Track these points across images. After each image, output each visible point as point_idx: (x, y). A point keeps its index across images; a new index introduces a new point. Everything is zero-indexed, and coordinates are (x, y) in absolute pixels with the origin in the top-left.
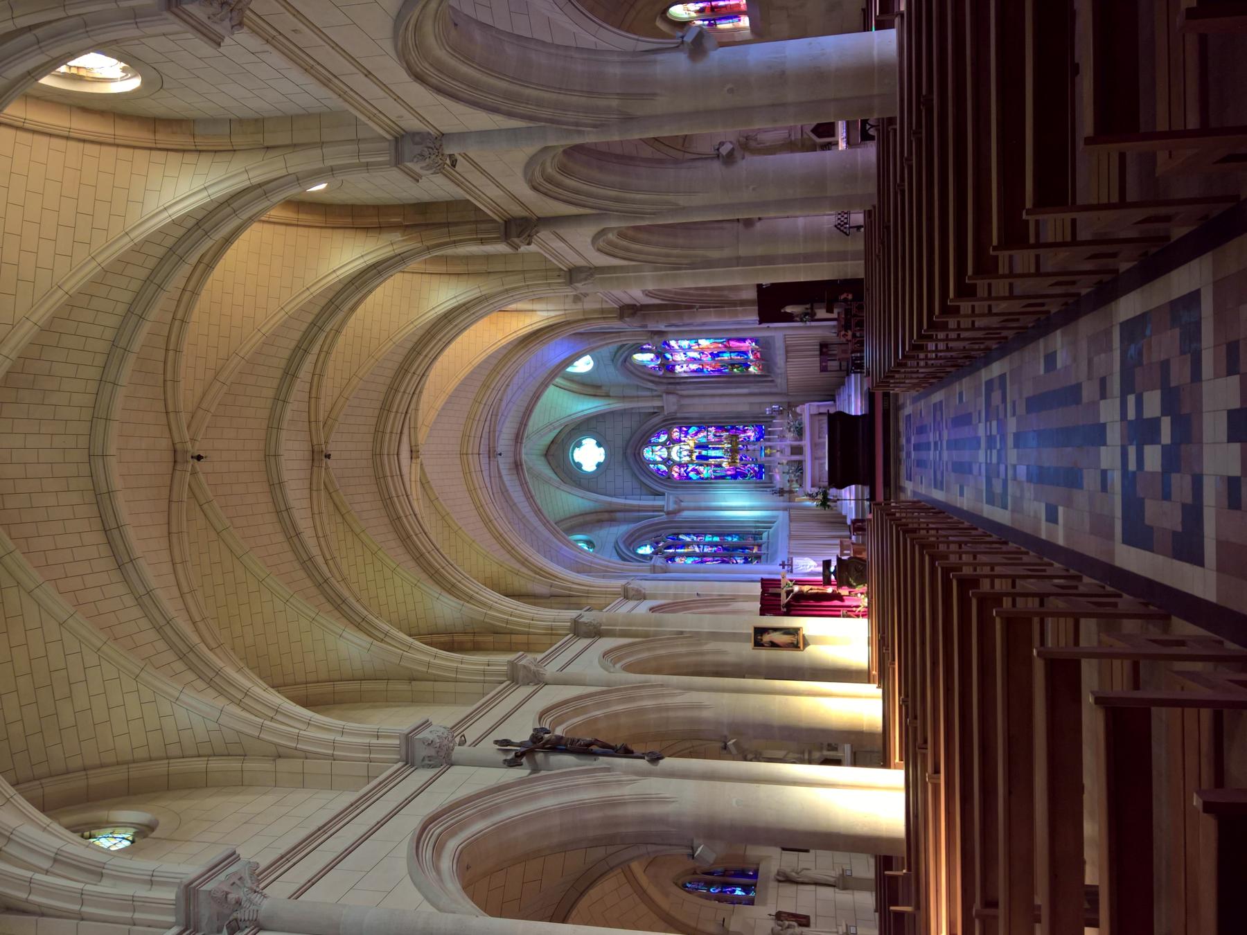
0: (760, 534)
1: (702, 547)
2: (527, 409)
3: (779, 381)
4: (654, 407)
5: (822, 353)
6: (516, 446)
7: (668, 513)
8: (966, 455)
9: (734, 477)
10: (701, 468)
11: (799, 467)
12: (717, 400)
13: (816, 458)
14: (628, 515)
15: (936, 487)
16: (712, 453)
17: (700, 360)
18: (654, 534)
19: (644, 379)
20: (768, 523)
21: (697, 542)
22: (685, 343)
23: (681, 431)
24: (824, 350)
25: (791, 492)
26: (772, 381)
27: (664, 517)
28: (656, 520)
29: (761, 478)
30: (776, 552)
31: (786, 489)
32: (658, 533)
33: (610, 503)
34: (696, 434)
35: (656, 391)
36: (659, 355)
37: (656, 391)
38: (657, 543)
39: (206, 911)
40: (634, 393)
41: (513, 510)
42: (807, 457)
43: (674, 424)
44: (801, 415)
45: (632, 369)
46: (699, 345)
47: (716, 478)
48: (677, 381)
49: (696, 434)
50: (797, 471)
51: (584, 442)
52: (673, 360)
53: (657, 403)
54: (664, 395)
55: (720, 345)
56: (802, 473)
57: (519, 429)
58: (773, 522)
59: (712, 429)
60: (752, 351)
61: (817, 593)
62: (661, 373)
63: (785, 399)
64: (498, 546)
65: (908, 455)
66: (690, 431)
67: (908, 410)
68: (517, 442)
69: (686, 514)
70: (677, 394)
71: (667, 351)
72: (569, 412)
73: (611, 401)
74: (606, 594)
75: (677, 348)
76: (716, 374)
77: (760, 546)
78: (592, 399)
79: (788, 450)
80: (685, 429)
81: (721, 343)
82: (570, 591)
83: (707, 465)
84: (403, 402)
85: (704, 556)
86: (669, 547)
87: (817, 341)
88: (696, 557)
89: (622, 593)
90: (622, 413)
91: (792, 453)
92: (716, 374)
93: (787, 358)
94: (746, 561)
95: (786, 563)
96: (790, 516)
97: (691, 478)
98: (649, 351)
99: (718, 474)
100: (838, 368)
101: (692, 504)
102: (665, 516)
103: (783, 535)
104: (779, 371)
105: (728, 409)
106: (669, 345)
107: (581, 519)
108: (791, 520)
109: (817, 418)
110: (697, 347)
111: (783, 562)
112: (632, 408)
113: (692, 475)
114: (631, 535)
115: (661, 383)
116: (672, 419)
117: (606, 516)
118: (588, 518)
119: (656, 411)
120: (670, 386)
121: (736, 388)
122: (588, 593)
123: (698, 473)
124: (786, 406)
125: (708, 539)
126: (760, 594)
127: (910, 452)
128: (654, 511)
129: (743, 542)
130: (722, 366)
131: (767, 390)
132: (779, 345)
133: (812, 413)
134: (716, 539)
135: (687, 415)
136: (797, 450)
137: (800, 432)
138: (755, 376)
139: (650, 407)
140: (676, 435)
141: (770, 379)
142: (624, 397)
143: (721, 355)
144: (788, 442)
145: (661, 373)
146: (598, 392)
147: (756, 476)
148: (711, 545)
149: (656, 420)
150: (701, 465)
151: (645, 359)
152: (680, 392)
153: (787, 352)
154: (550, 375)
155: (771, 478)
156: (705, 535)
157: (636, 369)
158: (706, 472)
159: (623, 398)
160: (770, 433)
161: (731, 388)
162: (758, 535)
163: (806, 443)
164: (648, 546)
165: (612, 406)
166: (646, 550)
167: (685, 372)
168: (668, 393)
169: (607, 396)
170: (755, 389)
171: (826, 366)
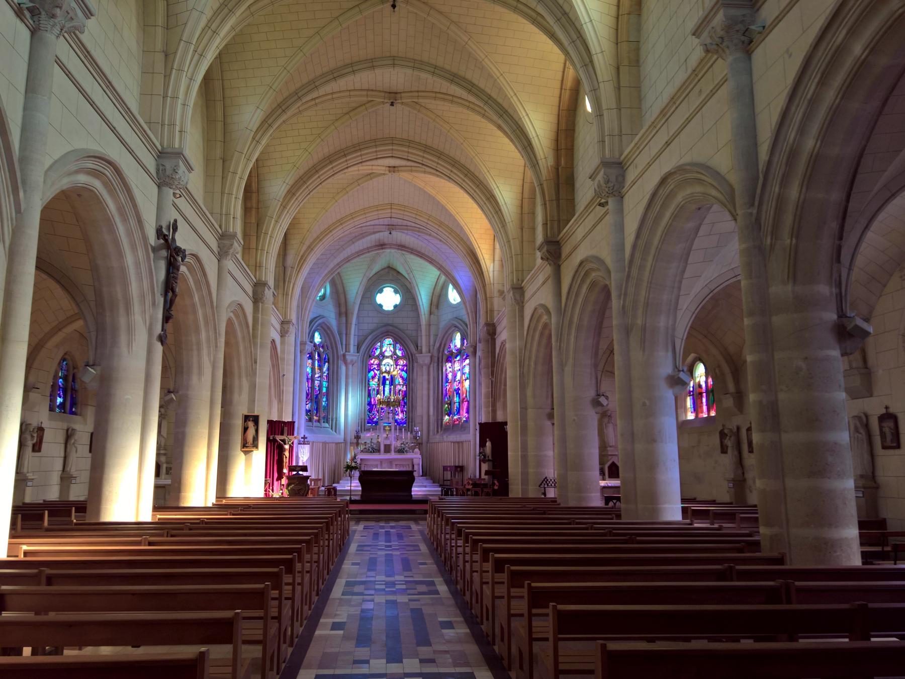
1: (319, 379)
4: (421, 347)
5: (456, 467)
7: (344, 355)
8: (381, 567)
9: (370, 404)
10: (376, 380)
12: (425, 392)
13: (381, 462)
15: (359, 546)
16: (387, 388)
18: (329, 345)
19: (442, 339)
20: (335, 427)
22: (467, 370)
23: (403, 366)
25: (358, 444)
26: (438, 432)
27: (341, 352)
28: (339, 346)
29: (368, 423)
31: (360, 441)
34: (401, 377)
35: (434, 348)
36: (459, 352)
37: (434, 348)
40: (432, 333)
43: (409, 361)
44: (413, 452)
45: (450, 331)
46: (465, 380)
47: (369, 391)
48: (440, 364)
49: (401, 377)
50: (373, 448)
52: (455, 361)
53: (424, 350)
54: (430, 354)
55: (464, 395)
56: (371, 452)
59: (404, 389)
62: (446, 352)
65: (382, 527)
67: (414, 527)
69: (343, 368)
70: (431, 364)
71: (462, 357)
72: (420, 285)
73: (427, 316)
75: (464, 364)
77: (319, 421)
79: (388, 442)
80: (405, 369)
81: (466, 396)
83: (379, 384)
86: (319, 355)
88: (312, 376)
89: (285, 320)
91: (385, 445)
92: (444, 392)
94: (308, 411)
97: (369, 372)
98: (462, 344)
101: (350, 373)
102: (342, 353)
104: (445, 437)
105: (419, 400)
106: (466, 359)
107: (340, 290)
108: (337, 444)
109: (410, 463)
110: (464, 378)
111: (306, 438)
112: (421, 331)
113: (372, 373)
114: (329, 328)
115: (439, 353)
116: (413, 360)
117: (343, 310)
118: (342, 297)
120: (436, 359)
122: (286, 295)
123: (373, 378)
124: (420, 441)
125: (325, 384)
127: (384, 529)
128: (346, 345)
129: (322, 409)
130: (449, 396)
131: (431, 428)
134: (324, 390)
136: (388, 449)
137: (400, 451)
138: (442, 420)
139: (421, 343)
141: (439, 430)
142: (430, 325)
143: (458, 395)
147: (370, 419)
148: (320, 386)
150: (379, 380)
152: (432, 365)
153: (458, 443)
155: (368, 430)
156: (328, 382)
158: (373, 383)
159: (429, 325)
160: (400, 430)
164: (320, 340)
165: (423, 316)
166: (317, 339)
167: (446, 369)
168: (431, 357)
169: (431, 313)
170: (432, 419)
171: (447, 470)
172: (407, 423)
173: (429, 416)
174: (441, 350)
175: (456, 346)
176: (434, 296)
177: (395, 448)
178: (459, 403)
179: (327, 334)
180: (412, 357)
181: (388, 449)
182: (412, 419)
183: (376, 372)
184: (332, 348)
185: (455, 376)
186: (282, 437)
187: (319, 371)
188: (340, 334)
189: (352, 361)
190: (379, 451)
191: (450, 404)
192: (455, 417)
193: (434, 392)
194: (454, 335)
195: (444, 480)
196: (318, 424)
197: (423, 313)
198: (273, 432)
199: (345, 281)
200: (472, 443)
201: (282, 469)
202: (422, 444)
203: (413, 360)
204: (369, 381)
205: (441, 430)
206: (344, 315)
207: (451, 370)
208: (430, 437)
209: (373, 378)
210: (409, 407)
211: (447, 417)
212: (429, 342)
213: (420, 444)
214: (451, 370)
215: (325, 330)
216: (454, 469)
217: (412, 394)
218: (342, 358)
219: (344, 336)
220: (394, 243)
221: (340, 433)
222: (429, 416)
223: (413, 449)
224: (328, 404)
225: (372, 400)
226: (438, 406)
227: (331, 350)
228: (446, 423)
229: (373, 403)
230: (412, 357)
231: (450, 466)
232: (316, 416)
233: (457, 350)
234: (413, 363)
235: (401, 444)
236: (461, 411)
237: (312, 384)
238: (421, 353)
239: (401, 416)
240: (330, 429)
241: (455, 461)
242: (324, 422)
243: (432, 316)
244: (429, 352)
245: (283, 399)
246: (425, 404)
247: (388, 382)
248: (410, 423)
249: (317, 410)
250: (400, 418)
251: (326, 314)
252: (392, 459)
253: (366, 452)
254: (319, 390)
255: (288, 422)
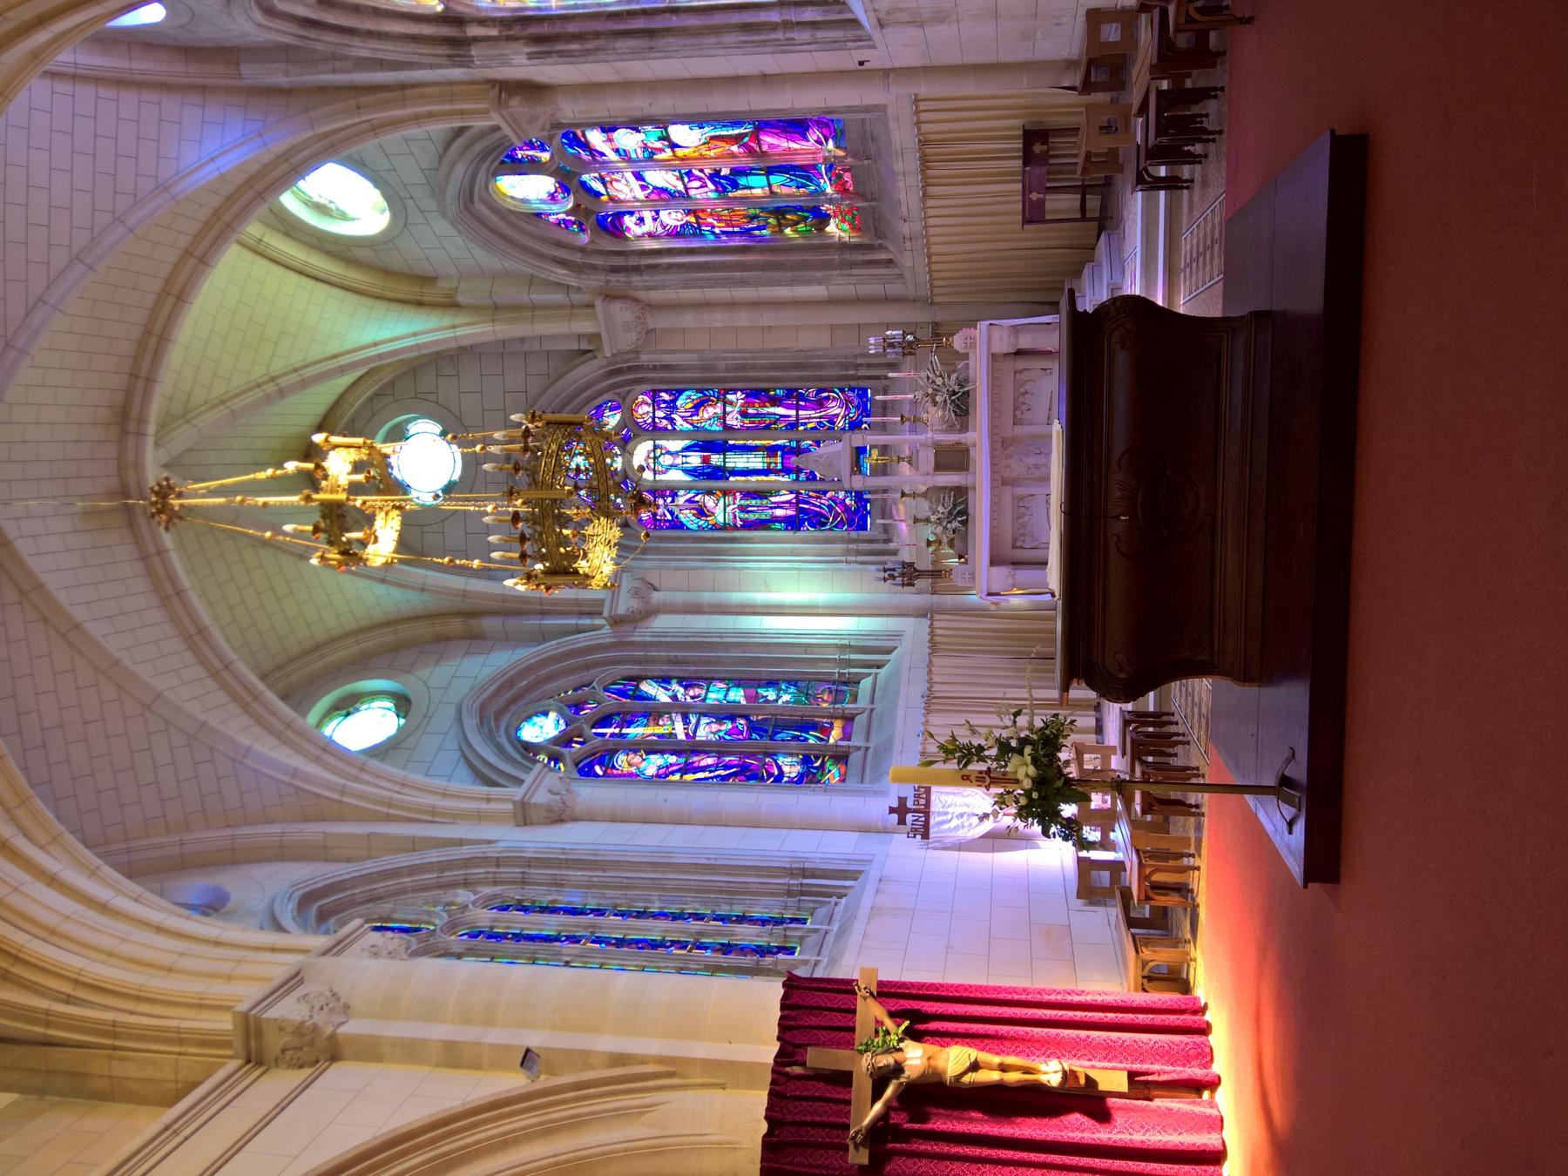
0: (854, 682)
1: (693, 719)
2: (147, 331)
3: (907, 261)
4: (579, 337)
5: (1028, 158)
6: (121, 442)
7: (616, 621)
9: (792, 524)
10: (709, 502)
11: (958, 506)
12: (742, 319)
13: (1004, 483)
14: (513, 624)
16: (737, 461)
17: (685, 195)
18: (575, 679)
19: (541, 256)
20: (875, 652)
21: (685, 705)
22: (628, 140)
23: (656, 403)
24: (1038, 148)
25: (936, 574)
26: (890, 262)
27: (606, 634)
28: (582, 640)
29: (863, 527)
30: (888, 746)
31: (924, 564)
32: (586, 676)
33: (465, 594)
34: (697, 407)
35: (579, 290)
36: (567, 182)
37: (579, 290)
38: (578, 707)
39: (251, 1020)
40: (521, 295)
41: (71, 645)
42: (980, 478)
43: (638, 381)
44: (966, 356)
45: (494, 220)
46: (674, 146)
47: (748, 525)
48: (633, 261)
49: (697, 407)
50: (951, 516)
51: (413, 428)
52: (612, 199)
53: (584, 326)
54: (598, 303)
55: (735, 148)
56: (964, 523)
57: (129, 393)
58: (889, 651)
59: (737, 398)
60: (830, 168)
61: (999, 1087)
62: (584, 238)
63: (922, 316)
64: (222, 697)
66: (679, 403)
68: (124, 432)
69: (662, 623)
70: (636, 300)
71: (587, 167)
72: (334, 347)
73: (460, 319)
74: (182, 1042)
75: (612, 156)
76: (737, 242)
77: (849, 719)
78: (409, 311)
79: (927, 458)
80: (666, 397)
81: (737, 139)
82: (47, 1024)
83: (725, 493)
84: (311, 368)
85: (695, 752)
86: (605, 721)
87: (1016, 124)
88: (673, 753)
89: (238, 1043)
90: (501, 350)
91: (939, 467)
92: (737, 242)
93: (926, 185)
94: (809, 776)
95: (910, 804)
96: (932, 634)
97: (681, 526)
98: (533, 167)
99: (751, 517)
100: (1079, 216)
101: (680, 597)
102: (607, 630)
103: (912, 692)
104: (905, 229)
105: (774, 342)
106: (586, 146)
107: (387, 637)
108: (934, 647)
109: (1011, 365)
110: (668, 154)
111: (902, 801)
112: (522, 340)
113: (687, 517)
114: (511, 683)
115: (593, 267)
116: (631, 369)
117: (455, 626)
118: (408, 632)
119: (584, 346)
120: (613, 278)
121: (793, 282)
122: (116, 1036)
123: (701, 512)
124: (925, 334)
125: (715, 695)
126: (770, 1060)
128: (582, 614)
129: (806, 708)
130: (752, 218)
131: (875, 289)
132: (902, 136)
133: (996, 350)
134: (737, 695)
135: (668, 359)
136: (952, 458)
137: (961, 406)
138: (843, 246)
139: (566, 337)
140: (644, 411)
141: (883, 256)
142: (496, 307)
143: (742, 181)
144: (930, 436)
145: (584, 238)
146: (429, 294)
147: (850, 523)
148: (722, 714)
149: (588, 370)
150: (710, 493)
151: (532, 196)
152: (641, 295)
153: (925, 162)
154: (207, 226)
155: (888, 533)
156: (710, 680)
157: (512, 225)
158: (721, 510)
159: (495, 310)
160: (885, 408)
161: (779, 283)
162: (844, 686)
163: (978, 437)
164: (553, 715)
165: (460, 332)
166: (542, 729)
167: (651, 235)
168: (610, 297)
169: (450, 305)
170: (841, 286)
171: (1040, 204)
172: (863, 384)
173: (832, 302)
174: (577, 257)
175: (552, 197)
176: (390, 294)
177: (951, 428)
178: (769, 171)
179: (530, 688)
180: (619, 371)
181: (952, 458)
182: (846, 366)
183: (681, 501)
184: (588, 667)
185: (663, 196)
186: (862, 1085)
187: (664, 721)
188: (543, 636)
189: (636, 593)
190: (960, 492)
191: (779, 212)
192: (829, 190)
193: (742, 283)
194: (510, 205)
195: (1083, 218)
196: (860, 721)
197: (449, 334)
198: (818, 1135)
199: (350, 624)
200: (924, 89)
201: (1039, 1090)
202: (936, 325)
203: (631, 369)
204: (716, 527)
205: (881, 247)
206: (473, 622)
207: (648, 215)
208: (910, 292)
209: (701, 512)
210: (801, 379)
211: (832, 228)
212: (560, 307)
213: (937, 335)
214: (648, 215)
215: (513, 701)
216: (1039, 171)
217: (753, 368)
218: (628, 628)
219: (550, 621)
220: (111, 451)
221: (897, 635)
222: (832, 302)
223: (953, 359)
224: (792, 682)
225: (779, 512)
226: (794, 267)
227: (593, 672)
228: (853, 228)
229: (790, 512)
230: (619, 371)
231: (1025, 192)
232: (827, 731)
233: (565, 189)
234: (640, 368)
235: (935, 404)
236: (800, 161)
237: (707, 753)
238: (595, 337)
239: (834, 409)
240: (882, 671)
241: (1005, 177)
242: (855, 699)
243: (461, 299)
244: (591, 306)
245: (660, 1060)
246: (789, 317)
247: (716, 459)
248: (863, 372)
249: (806, 726)
250: (842, 412)
251: (460, 690)
252: (992, 442)
253: (965, 539)
254: (732, 718)
255: (785, 1005)
